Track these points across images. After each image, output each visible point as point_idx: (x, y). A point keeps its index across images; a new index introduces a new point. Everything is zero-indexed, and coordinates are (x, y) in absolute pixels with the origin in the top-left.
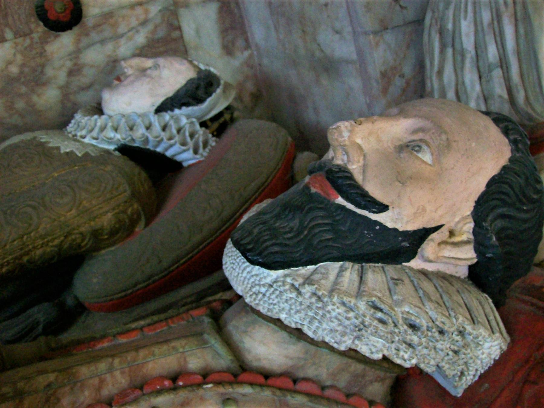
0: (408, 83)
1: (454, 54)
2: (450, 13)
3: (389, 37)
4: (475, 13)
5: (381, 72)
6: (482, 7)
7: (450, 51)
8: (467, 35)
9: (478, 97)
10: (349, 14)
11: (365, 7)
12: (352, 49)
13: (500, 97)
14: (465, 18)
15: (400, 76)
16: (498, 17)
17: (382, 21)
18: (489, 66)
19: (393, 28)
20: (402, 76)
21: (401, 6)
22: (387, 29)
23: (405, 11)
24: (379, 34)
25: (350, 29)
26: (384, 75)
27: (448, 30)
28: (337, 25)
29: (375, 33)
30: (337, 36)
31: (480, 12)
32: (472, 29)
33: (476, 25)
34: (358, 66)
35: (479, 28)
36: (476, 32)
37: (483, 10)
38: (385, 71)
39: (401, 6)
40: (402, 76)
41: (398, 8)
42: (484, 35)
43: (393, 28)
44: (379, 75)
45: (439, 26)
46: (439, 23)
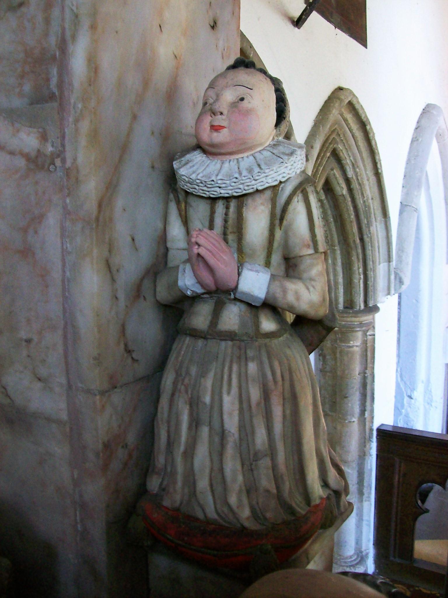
0: (130, 456)
1: (210, 436)
2: (208, 383)
3: (117, 398)
4: (240, 388)
5: (103, 443)
6: (250, 382)
7: (205, 431)
8: (230, 414)
9: (240, 491)
10: (67, 363)
11: (95, 359)
12: (63, 405)
13: (267, 491)
14: (229, 393)
15: (123, 447)
16: (266, 395)
17: (111, 377)
18: (256, 454)
19: (121, 387)
20: (125, 446)
21: (132, 358)
22: (116, 388)
23: (136, 365)
24: (107, 394)
25: (63, 380)
26: (106, 446)
27: (205, 404)
28: (43, 372)
29: (102, 393)
30: (39, 385)
31: (247, 388)
32: (237, 406)
33: (241, 402)
34: (68, 430)
35: (245, 406)
36: (241, 410)
37: (250, 386)
38: (108, 441)
39: (132, 358)
40: (125, 446)
41: (129, 361)
42: (251, 417)
43: (121, 387)
44: (101, 446)
45: (190, 396)
46: (190, 392)
